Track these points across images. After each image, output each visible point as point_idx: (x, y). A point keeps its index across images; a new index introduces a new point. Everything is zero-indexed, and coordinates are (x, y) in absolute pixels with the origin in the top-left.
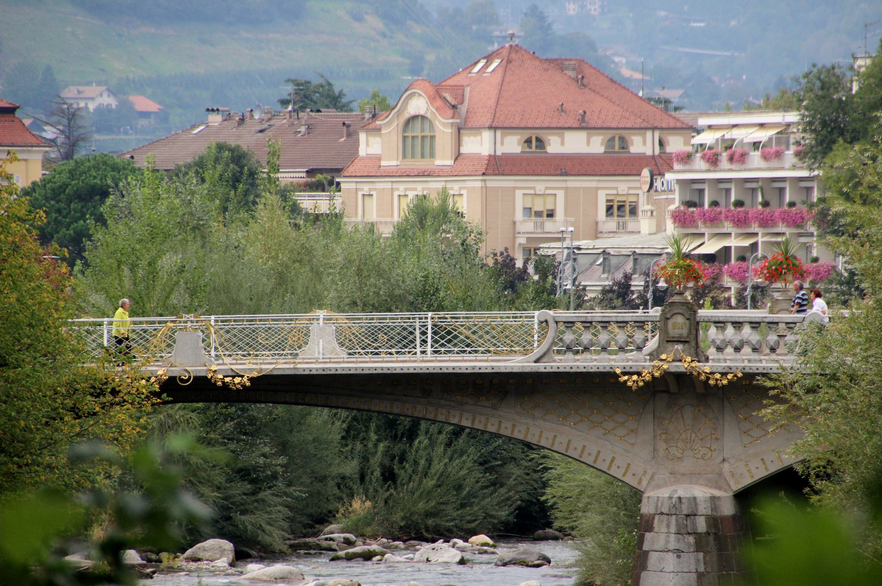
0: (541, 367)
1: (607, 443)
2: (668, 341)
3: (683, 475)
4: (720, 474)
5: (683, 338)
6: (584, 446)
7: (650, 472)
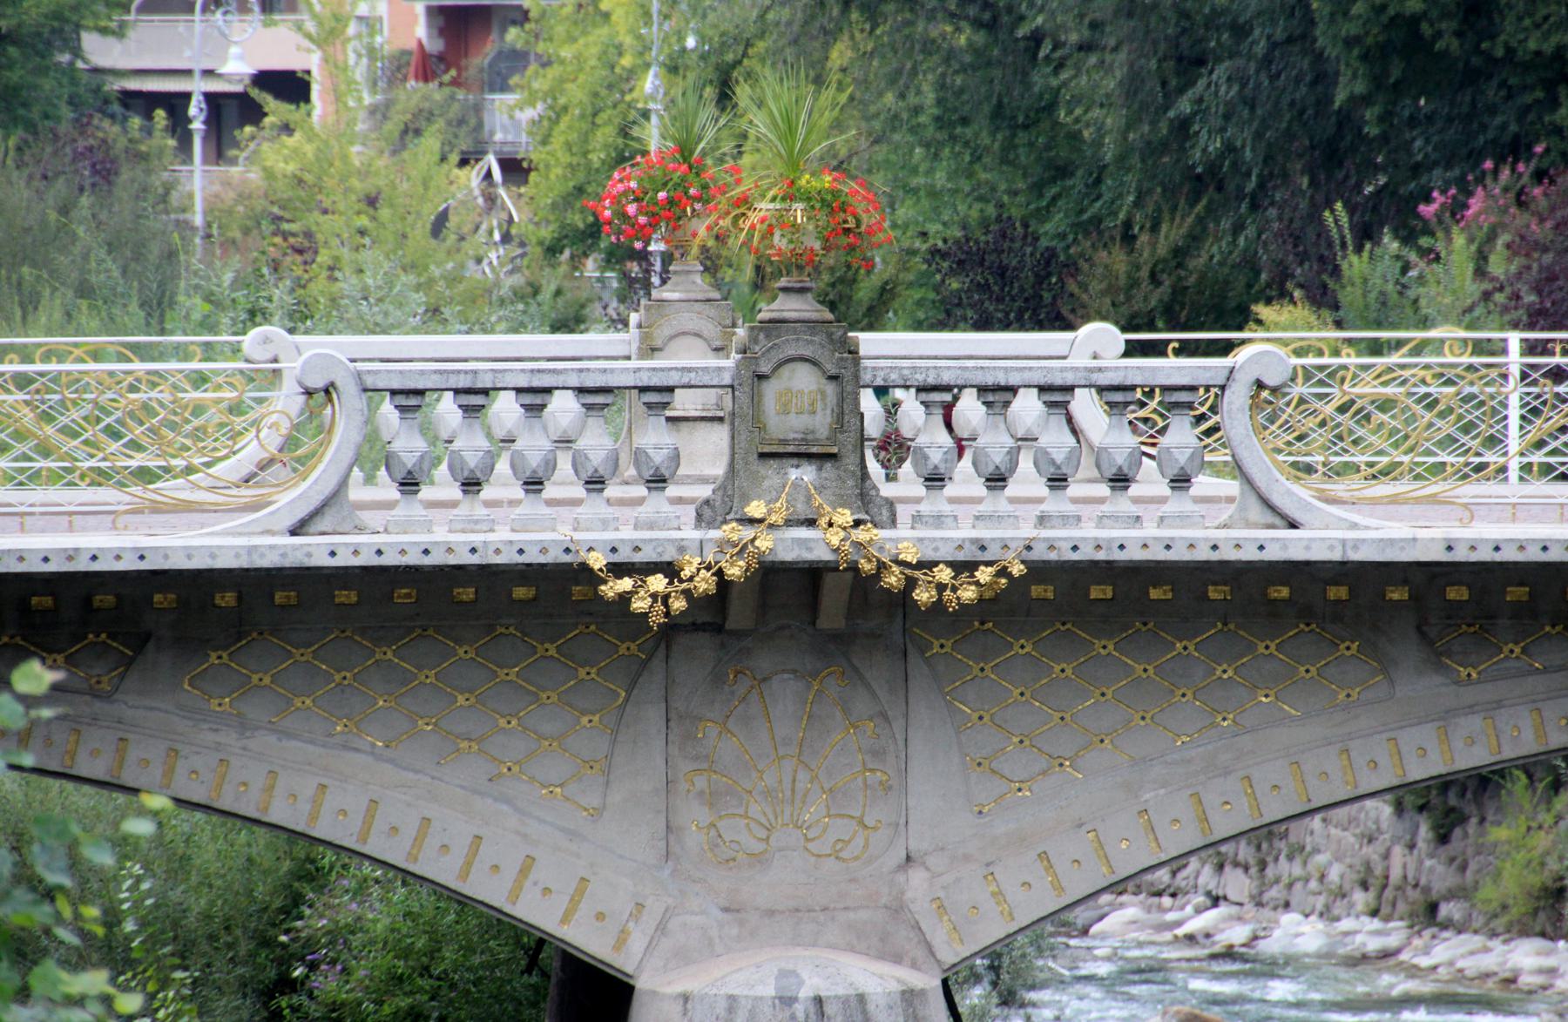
0: (315, 550)
1: (505, 808)
2: (763, 456)
3: (771, 913)
4: (897, 908)
5: (816, 442)
6: (426, 821)
7: (655, 908)
